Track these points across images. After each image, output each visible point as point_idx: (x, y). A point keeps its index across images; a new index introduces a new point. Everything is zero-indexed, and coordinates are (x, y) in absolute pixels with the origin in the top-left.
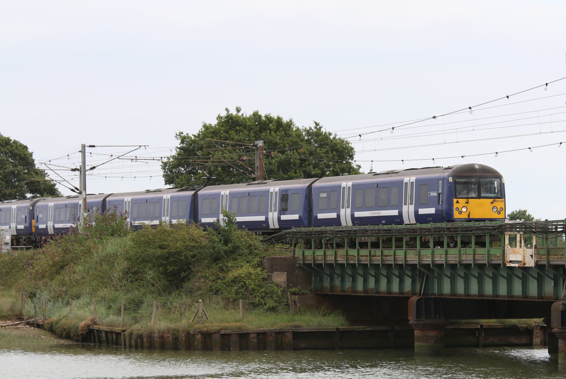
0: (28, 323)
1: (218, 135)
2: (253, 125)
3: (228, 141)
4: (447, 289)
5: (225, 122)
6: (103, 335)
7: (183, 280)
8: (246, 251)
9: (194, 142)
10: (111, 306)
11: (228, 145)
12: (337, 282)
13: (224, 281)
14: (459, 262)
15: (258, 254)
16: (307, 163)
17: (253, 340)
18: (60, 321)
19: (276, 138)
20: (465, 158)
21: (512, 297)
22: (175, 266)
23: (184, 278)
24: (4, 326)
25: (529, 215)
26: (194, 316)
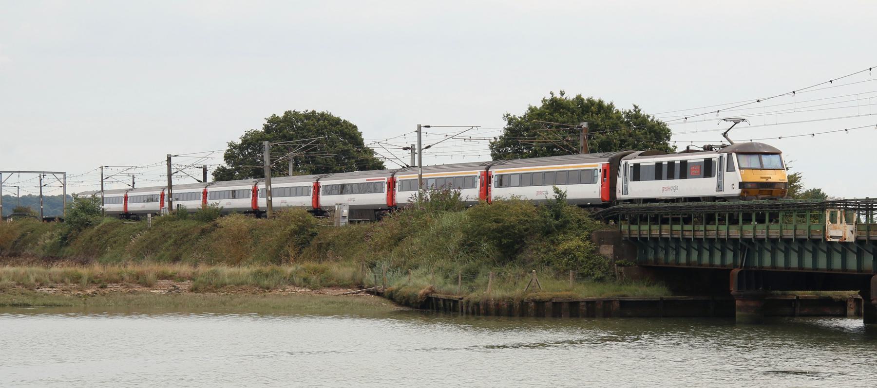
0: (368, 292)
1: (543, 117)
2: (576, 108)
3: (553, 123)
4: (767, 262)
5: (549, 104)
6: (441, 302)
7: (516, 252)
8: (575, 225)
9: (520, 123)
10: (448, 276)
11: (552, 126)
12: (661, 255)
13: (555, 253)
14: (781, 237)
15: (586, 228)
16: (626, 143)
18: (399, 289)
19: (598, 119)
20: (781, 139)
21: (789, 268)
22: (509, 239)
23: (517, 250)
24: (346, 294)
25: (823, 194)
26: (527, 285)
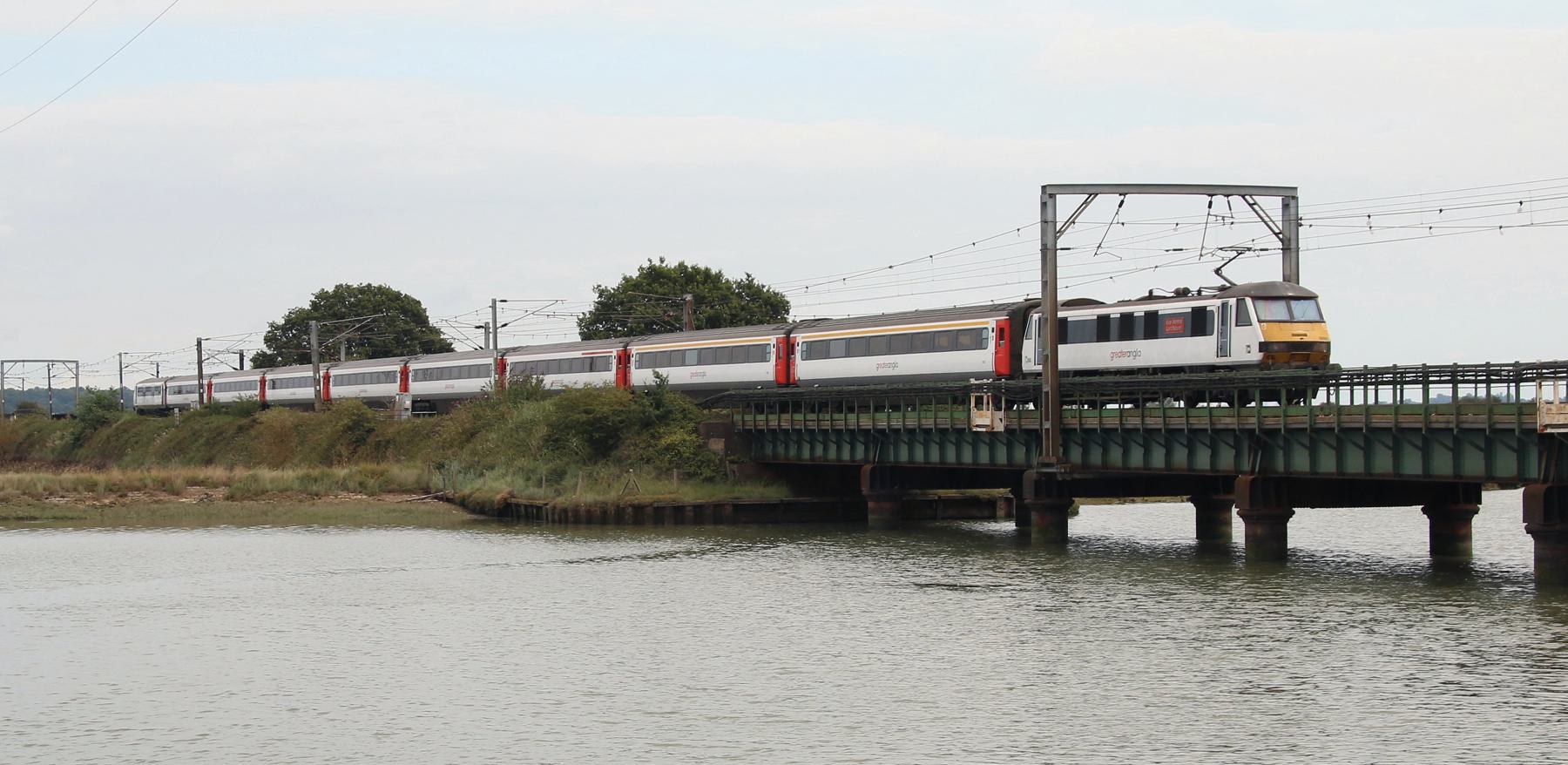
0: (436, 498)
4: (904, 456)
6: (523, 509)
7: (611, 448)
9: (613, 295)
14: (919, 427)
16: (738, 319)
17: (690, 514)
19: (704, 290)
